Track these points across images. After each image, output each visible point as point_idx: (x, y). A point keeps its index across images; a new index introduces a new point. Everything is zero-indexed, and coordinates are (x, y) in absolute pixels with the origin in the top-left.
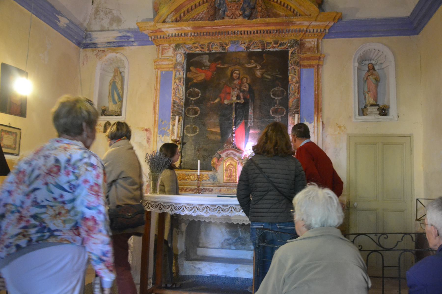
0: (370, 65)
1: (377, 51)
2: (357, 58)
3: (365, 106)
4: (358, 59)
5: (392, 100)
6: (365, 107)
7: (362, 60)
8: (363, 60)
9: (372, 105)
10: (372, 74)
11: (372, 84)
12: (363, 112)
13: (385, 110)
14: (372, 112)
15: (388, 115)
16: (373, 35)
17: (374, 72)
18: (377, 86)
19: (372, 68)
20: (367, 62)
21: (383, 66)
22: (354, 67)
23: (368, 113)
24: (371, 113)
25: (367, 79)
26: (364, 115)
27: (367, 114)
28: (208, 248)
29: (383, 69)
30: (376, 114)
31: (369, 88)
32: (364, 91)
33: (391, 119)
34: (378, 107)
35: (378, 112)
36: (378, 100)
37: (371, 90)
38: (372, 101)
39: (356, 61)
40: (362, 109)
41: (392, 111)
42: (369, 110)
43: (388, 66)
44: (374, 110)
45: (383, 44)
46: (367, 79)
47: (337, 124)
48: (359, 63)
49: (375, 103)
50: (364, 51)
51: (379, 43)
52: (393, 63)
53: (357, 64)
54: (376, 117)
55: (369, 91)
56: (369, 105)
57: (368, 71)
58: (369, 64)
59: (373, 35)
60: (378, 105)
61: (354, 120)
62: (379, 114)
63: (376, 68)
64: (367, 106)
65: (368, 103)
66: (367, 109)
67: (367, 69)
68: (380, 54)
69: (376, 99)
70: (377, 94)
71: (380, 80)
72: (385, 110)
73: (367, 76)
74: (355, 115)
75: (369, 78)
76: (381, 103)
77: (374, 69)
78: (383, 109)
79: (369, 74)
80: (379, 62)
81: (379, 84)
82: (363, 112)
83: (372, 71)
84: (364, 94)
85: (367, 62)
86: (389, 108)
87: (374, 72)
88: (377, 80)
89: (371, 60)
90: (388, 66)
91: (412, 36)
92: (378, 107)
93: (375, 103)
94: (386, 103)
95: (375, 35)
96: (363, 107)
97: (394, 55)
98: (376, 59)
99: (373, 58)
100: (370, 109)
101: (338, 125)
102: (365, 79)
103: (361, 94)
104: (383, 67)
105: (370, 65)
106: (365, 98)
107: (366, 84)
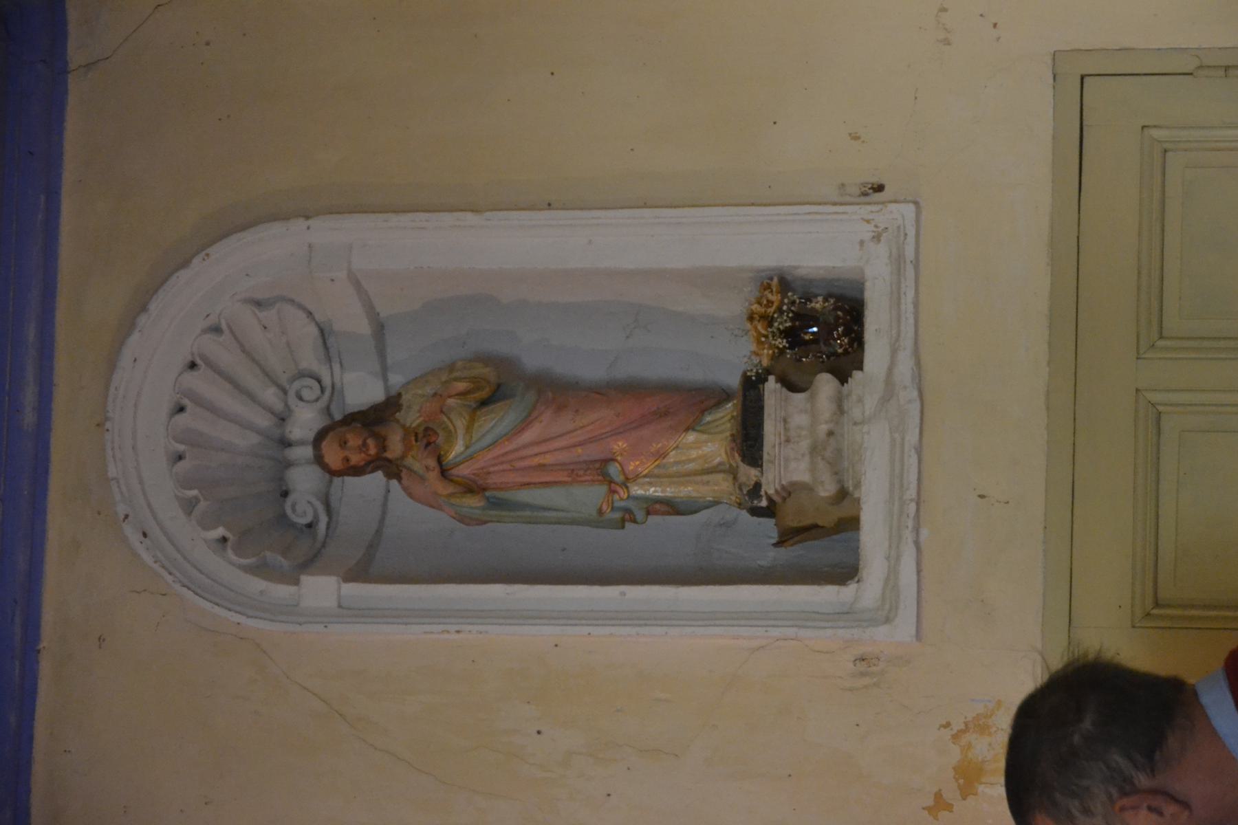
0: (333, 456)
1: (194, 381)
2: (257, 585)
3: (756, 512)
4: (262, 570)
5: (676, 257)
6: (770, 511)
7: (277, 536)
8: (282, 520)
9: (749, 443)
10: (427, 437)
11: (528, 436)
12: (814, 540)
13: (804, 318)
14: (814, 450)
15: (860, 286)
16: (29, 418)
17: (411, 417)
18: (555, 392)
19: (366, 436)
20: (305, 480)
21: (351, 320)
22: (347, 612)
23: (827, 489)
24: (833, 450)
25: (471, 488)
26: (851, 524)
27: (843, 494)
28: (379, 532)
29: (380, 329)
30: (840, 410)
31: (574, 473)
32: (599, 521)
33: (898, 261)
34: (771, 384)
35: (826, 384)
36: (696, 374)
37: (593, 452)
38: (708, 445)
39: (282, 591)
40: (787, 536)
41: (818, 246)
42: (799, 472)
43: (355, 282)
44: (800, 419)
45: (128, 326)
46: (471, 488)
47: (939, 804)
48: (308, 564)
49: (726, 416)
50: (189, 506)
51: (112, 364)
52: (329, 232)
53: (320, 589)
54: (871, 403)
55: (600, 469)
56: (749, 474)
57: (393, 470)
58: (319, 460)
59: (29, 418)
60: (752, 385)
61: (904, 628)
62: (843, 377)
63: (363, 391)
64: (756, 489)
65: (721, 485)
66: (788, 491)
67: (377, 479)
68: (222, 352)
69: (689, 402)
70: (632, 389)
71: (486, 359)
72: (804, 318)
73: (443, 489)
74: (847, 615)
75: (464, 471)
76: (731, 356)
77: (374, 419)
78: (793, 336)
79: (419, 462)
80: (310, 359)
81: (533, 361)
82: (814, 540)
83: (395, 446)
84: (627, 517)
85: (305, 480)
86: (784, 282)
87: (411, 417)
88: (495, 385)
89: (286, 443)
90: (355, 282)
91: (76, 55)
92: (771, 384)
93: (730, 409)
94: (735, 305)
95: (30, 396)
96: (768, 526)
97: (275, 219)
98: (270, 395)
99: (264, 421)
100: (788, 464)
101: (951, 794)
102: (473, 503)
103: (627, 552)
104: (364, 328)
105: (333, 456)
106: (672, 507)
107: (524, 496)
